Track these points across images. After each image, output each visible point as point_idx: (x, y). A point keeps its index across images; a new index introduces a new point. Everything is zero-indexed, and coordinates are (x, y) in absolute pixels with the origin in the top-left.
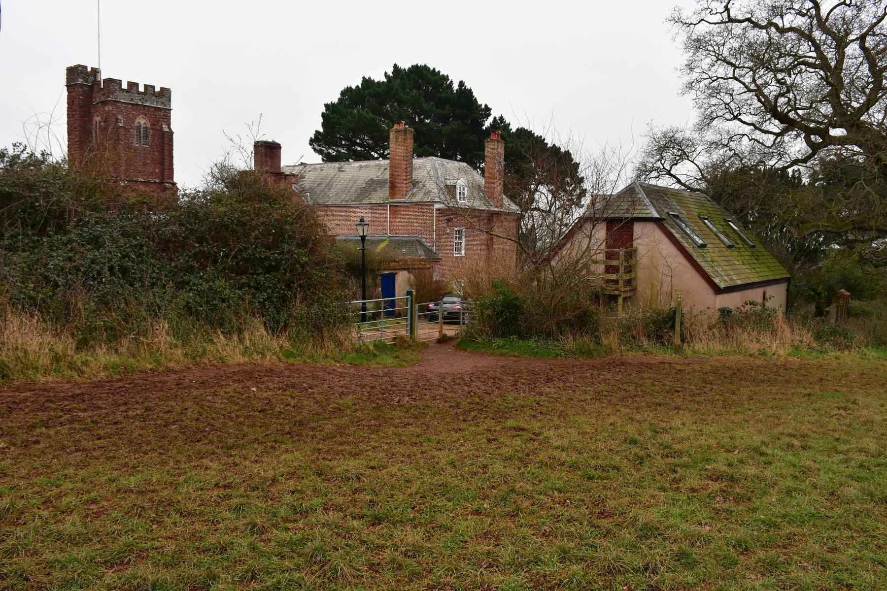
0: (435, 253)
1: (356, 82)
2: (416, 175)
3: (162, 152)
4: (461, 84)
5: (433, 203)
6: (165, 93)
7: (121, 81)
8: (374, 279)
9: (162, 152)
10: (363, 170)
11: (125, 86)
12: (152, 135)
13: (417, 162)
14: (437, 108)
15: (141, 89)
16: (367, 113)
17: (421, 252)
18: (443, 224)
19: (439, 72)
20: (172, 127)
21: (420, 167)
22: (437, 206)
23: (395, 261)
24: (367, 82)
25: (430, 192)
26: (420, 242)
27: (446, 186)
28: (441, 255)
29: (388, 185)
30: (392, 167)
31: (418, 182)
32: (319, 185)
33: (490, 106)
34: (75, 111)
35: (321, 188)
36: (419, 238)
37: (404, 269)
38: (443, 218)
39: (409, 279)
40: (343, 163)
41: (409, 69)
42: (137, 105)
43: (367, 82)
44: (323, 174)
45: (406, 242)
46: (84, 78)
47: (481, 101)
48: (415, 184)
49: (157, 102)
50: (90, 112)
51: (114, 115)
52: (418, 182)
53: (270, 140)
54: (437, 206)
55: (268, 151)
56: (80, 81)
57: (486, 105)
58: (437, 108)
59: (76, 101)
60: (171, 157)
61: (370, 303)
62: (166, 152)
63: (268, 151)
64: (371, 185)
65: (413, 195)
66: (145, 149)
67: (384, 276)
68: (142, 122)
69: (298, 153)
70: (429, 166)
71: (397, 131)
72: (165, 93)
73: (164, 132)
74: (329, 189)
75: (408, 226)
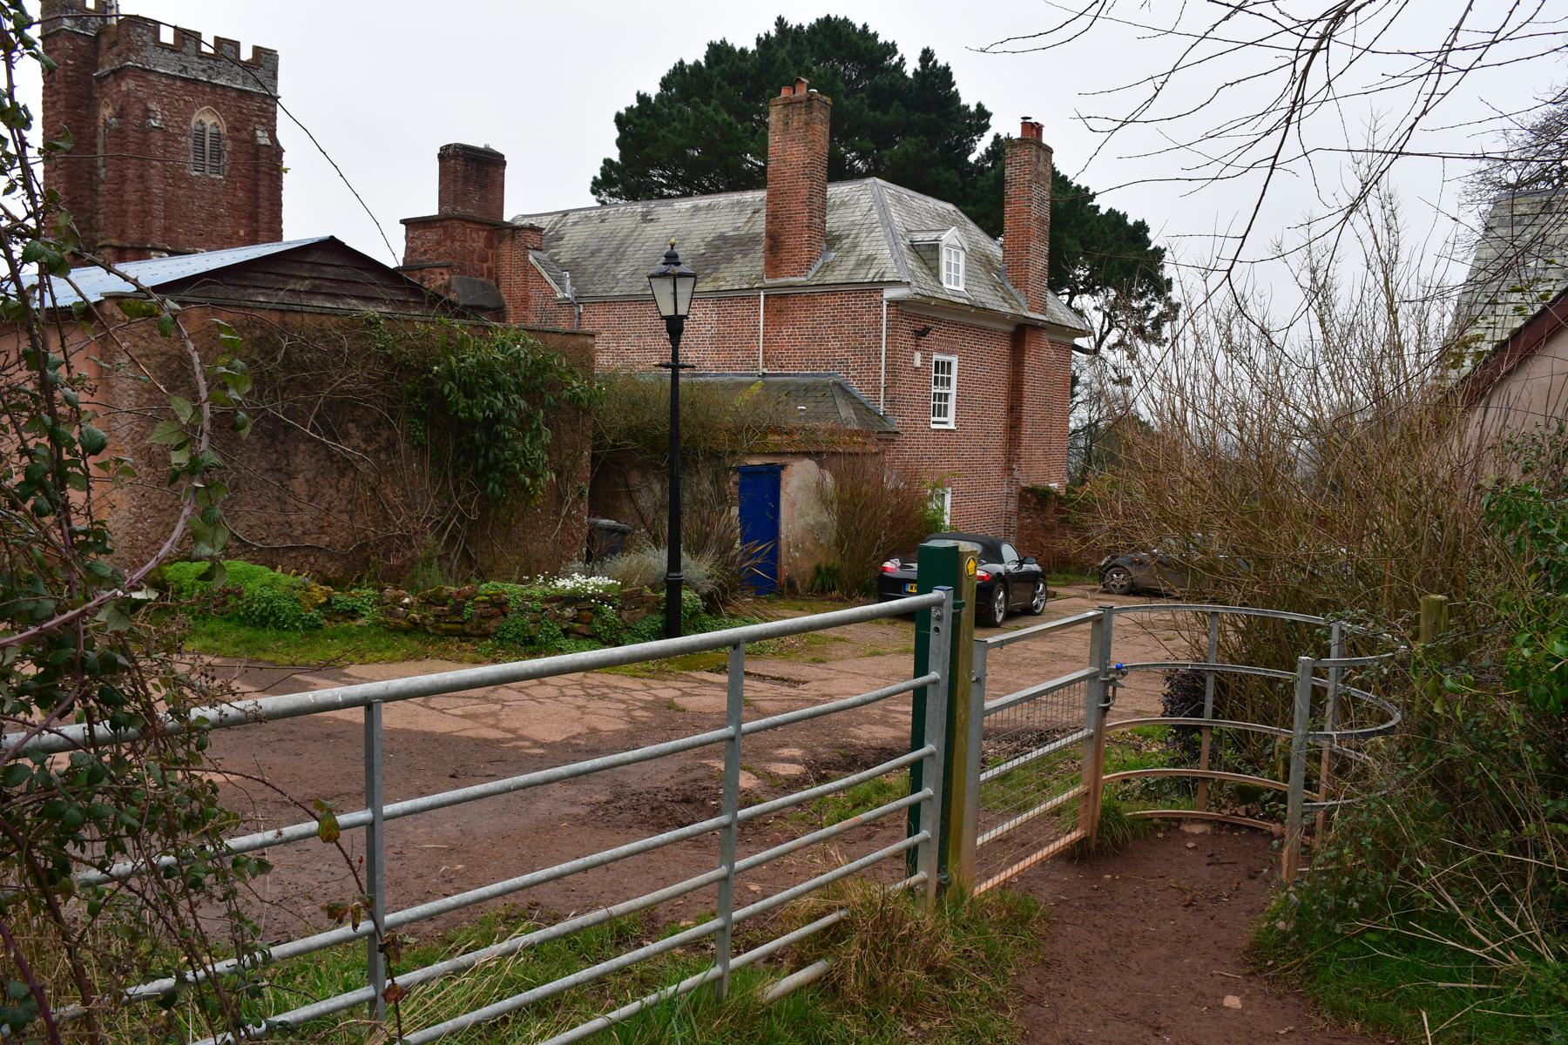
0: (883, 418)
1: (695, 54)
2: (833, 221)
3: (253, 192)
4: (927, 55)
5: (878, 285)
6: (265, 60)
8: (717, 480)
9: (253, 192)
10: (702, 214)
12: (232, 153)
16: (716, 110)
17: (846, 412)
18: (905, 339)
19: (875, 35)
20: (279, 135)
21: (843, 203)
22: (890, 293)
23: (777, 431)
24: (719, 52)
25: (870, 259)
26: (843, 390)
27: (913, 247)
28: (896, 423)
29: (761, 248)
31: (839, 238)
32: (593, 254)
33: (988, 108)
34: (58, 93)
35: (598, 260)
36: (841, 377)
37: (807, 454)
38: (906, 328)
39: (820, 484)
40: (653, 204)
41: (811, 27)
43: (719, 52)
44: (605, 228)
45: (807, 389)
47: (969, 97)
48: (832, 241)
49: (245, 79)
50: (91, 98)
51: (140, 100)
52: (839, 238)
53: (479, 143)
54: (890, 293)
55: (472, 171)
56: (67, 24)
57: (979, 106)
60: (277, 204)
61: (697, 568)
62: (263, 191)
63: (472, 171)
64: (719, 249)
65: (827, 267)
66: (213, 182)
67: (747, 472)
68: (209, 120)
69: (553, 178)
70: (866, 201)
71: (789, 104)
72: (265, 60)
73: (259, 147)
74: (618, 262)
75: (813, 350)
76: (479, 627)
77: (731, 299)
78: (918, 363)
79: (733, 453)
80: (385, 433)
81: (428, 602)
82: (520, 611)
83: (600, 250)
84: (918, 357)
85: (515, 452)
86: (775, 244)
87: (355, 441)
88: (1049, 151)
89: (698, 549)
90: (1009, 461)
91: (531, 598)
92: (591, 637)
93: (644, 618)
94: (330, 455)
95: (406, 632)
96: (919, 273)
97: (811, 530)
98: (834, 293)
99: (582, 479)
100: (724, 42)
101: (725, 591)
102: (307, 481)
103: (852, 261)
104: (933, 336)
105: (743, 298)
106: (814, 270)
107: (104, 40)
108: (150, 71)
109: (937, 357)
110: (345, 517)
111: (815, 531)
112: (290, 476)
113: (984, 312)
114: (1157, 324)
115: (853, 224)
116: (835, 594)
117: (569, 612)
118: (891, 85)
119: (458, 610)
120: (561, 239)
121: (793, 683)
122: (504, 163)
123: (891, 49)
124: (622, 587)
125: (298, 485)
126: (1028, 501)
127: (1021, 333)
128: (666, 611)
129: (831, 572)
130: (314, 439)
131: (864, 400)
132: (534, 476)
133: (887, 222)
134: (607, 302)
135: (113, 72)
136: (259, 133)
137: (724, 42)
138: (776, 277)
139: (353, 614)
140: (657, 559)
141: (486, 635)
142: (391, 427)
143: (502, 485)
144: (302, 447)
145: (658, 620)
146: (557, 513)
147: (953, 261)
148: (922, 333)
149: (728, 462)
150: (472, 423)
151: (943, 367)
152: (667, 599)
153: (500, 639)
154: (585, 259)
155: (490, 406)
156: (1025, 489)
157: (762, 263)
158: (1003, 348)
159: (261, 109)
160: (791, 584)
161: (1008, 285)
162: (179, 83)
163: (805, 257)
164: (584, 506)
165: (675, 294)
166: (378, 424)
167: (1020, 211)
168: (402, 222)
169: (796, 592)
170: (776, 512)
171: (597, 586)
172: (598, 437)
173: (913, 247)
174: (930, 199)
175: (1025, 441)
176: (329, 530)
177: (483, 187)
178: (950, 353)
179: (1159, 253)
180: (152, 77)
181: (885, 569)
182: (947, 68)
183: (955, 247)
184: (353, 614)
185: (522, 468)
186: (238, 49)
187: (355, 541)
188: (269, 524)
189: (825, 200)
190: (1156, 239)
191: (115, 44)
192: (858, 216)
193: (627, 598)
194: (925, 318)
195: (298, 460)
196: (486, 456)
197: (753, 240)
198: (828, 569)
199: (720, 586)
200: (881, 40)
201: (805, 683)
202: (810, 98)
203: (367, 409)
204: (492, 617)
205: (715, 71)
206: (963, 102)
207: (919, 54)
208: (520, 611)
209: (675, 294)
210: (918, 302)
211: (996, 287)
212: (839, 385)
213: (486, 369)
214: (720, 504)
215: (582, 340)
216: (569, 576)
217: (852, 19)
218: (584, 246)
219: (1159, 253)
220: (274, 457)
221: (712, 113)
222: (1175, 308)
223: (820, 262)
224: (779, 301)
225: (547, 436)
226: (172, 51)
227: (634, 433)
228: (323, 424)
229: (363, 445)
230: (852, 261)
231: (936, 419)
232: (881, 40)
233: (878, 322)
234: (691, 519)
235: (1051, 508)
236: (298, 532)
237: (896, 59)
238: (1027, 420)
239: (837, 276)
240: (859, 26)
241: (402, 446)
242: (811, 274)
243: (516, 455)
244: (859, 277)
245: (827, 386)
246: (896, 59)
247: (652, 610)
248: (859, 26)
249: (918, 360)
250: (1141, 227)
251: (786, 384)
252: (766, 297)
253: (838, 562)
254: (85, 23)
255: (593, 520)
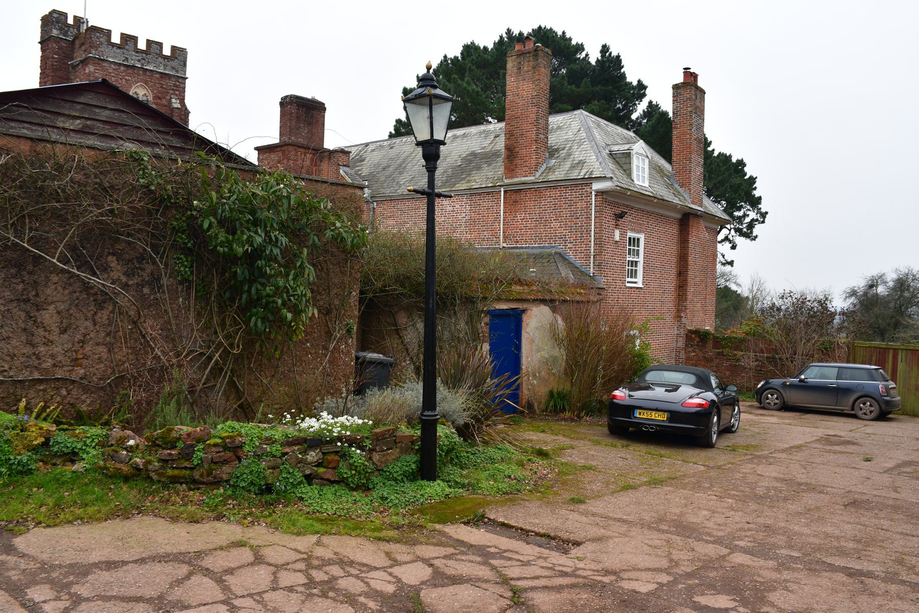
0: (593, 278)
1: (455, 51)
4: (605, 49)
5: (589, 180)
6: (179, 54)
7: (109, 32)
8: (471, 321)
11: (116, 39)
13: (555, 120)
14: (569, 83)
15: (142, 45)
17: (565, 272)
18: (609, 221)
19: (570, 39)
20: (186, 101)
21: (559, 128)
22: (596, 186)
23: (519, 282)
25: (581, 163)
26: (562, 257)
27: (611, 154)
28: (602, 281)
29: (501, 159)
30: (510, 135)
32: (384, 169)
33: (645, 83)
35: (387, 173)
36: (560, 248)
37: (543, 301)
38: (609, 212)
39: (553, 327)
42: (133, 67)
44: (393, 153)
46: (61, 29)
47: (632, 78)
48: (553, 152)
49: (165, 66)
52: (557, 150)
53: (308, 95)
54: (596, 186)
56: (55, 32)
57: (639, 81)
58: (569, 83)
59: (49, 63)
63: (302, 114)
64: (471, 161)
65: (549, 169)
67: (496, 315)
69: (360, 121)
70: (575, 125)
71: (521, 54)
72: (179, 54)
74: (401, 173)
76: (209, 473)
77: (479, 194)
78: (617, 238)
79: (485, 298)
80: (149, 268)
81: (154, 445)
82: (256, 455)
83: (389, 166)
84: (617, 234)
85: (278, 288)
86: (511, 154)
87: (115, 275)
88: (703, 92)
89: (454, 382)
90: (678, 311)
91: (270, 441)
92: (338, 482)
93: (397, 459)
94: (87, 287)
95: (126, 479)
96: (617, 172)
97: (545, 362)
98: (555, 187)
99: (350, 317)
100: (473, 43)
101: (478, 420)
102: (59, 313)
103: (568, 164)
104: (627, 218)
105: (488, 193)
106: (540, 171)
107: (77, 42)
108: (103, 60)
109: (630, 234)
110: (103, 350)
111: (549, 362)
112: (39, 308)
113: (663, 203)
114: (751, 226)
115: (567, 140)
116: (568, 414)
117: (313, 456)
118: (581, 68)
119: (187, 454)
120: (364, 160)
121: (564, 544)
122: (325, 109)
123: (580, 48)
124: (376, 425)
125: (49, 316)
126: (693, 340)
127: (686, 219)
128: (421, 451)
129: (562, 396)
130: (63, 270)
131: (578, 265)
132: (297, 312)
133: (592, 139)
134: (391, 199)
135: (82, 62)
136: (173, 100)
137: (473, 43)
138: (512, 177)
139: (72, 457)
140: (411, 393)
141: (217, 483)
142: (154, 263)
143: (264, 319)
144: (55, 278)
145: (411, 461)
146: (325, 348)
147: (641, 165)
148: (620, 216)
149: (480, 306)
150: (233, 259)
151: (634, 242)
152: (423, 437)
153: (235, 487)
154: (378, 173)
155: (250, 241)
156: (690, 331)
157: (502, 169)
158: (674, 230)
159: (175, 85)
160: (530, 406)
161: (676, 186)
162: (122, 68)
163: (533, 162)
164: (352, 341)
165: (431, 117)
166: (141, 258)
167: (684, 134)
168: (256, 149)
169: (534, 412)
170: (519, 347)
171: (343, 426)
172: (366, 280)
173: (611, 154)
174: (618, 128)
175: (690, 297)
176: (84, 362)
177: (310, 124)
178: (639, 232)
179: (752, 180)
180: (105, 64)
181: (615, 397)
182: (618, 57)
183: (641, 155)
184: (72, 457)
185: (284, 304)
186: (161, 48)
187: (113, 373)
188: (13, 356)
189: (547, 124)
190: (749, 171)
191: (83, 44)
192: (570, 135)
193: (378, 439)
194: (622, 204)
195: (48, 291)
196: (249, 291)
197: (496, 154)
198: (559, 394)
199: (474, 417)
200: (574, 42)
201: (577, 544)
202: (536, 50)
203: (129, 243)
204: (226, 462)
205: (467, 61)
206: (628, 80)
207: (600, 48)
208: (256, 455)
209: (431, 117)
210: (618, 192)
211: (669, 186)
212: (560, 254)
213: (248, 205)
214: (474, 340)
215: (350, 191)
216: (317, 417)
217: (555, 29)
218: (378, 165)
219: (752, 180)
220: (20, 287)
221: (465, 85)
222: (764, 215)
223: (544, 167)
224: (515, 195)
225: (310, 272)
226: (119, 48)
227: (402, 280)
228: (76, 255)
229: (124, 279)
230: (568, 164)
231: (628, 280)
232: (574, 42)
233: (588, 207)
234: (449, 353)
235: (710, 344)
236: (48, 364)
237: (583, 55)
238: (691, 281)
239: (558, 175)
240: (560, 33)
241: (165, 281)
242: (538, 174)
243: (278, 291)
244: (574, 175)
245: (550, 255)
246: (583, 55)
247: (406, 451)
248: (560, 33)
249: (617, 235)
250: (741, 163)
251: (519, 255)
252: (505, 192)
253: (568, 386)
254: (67, 32)
255: (362, 354)
